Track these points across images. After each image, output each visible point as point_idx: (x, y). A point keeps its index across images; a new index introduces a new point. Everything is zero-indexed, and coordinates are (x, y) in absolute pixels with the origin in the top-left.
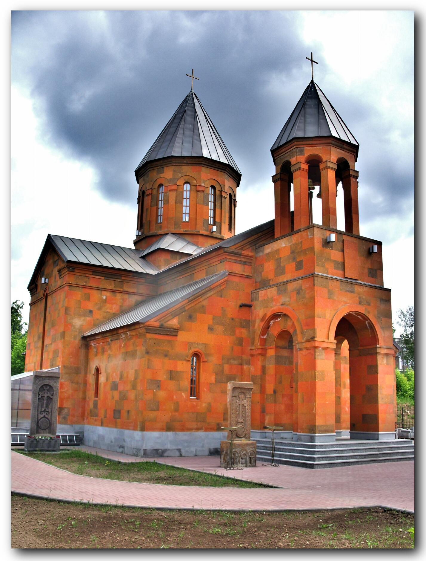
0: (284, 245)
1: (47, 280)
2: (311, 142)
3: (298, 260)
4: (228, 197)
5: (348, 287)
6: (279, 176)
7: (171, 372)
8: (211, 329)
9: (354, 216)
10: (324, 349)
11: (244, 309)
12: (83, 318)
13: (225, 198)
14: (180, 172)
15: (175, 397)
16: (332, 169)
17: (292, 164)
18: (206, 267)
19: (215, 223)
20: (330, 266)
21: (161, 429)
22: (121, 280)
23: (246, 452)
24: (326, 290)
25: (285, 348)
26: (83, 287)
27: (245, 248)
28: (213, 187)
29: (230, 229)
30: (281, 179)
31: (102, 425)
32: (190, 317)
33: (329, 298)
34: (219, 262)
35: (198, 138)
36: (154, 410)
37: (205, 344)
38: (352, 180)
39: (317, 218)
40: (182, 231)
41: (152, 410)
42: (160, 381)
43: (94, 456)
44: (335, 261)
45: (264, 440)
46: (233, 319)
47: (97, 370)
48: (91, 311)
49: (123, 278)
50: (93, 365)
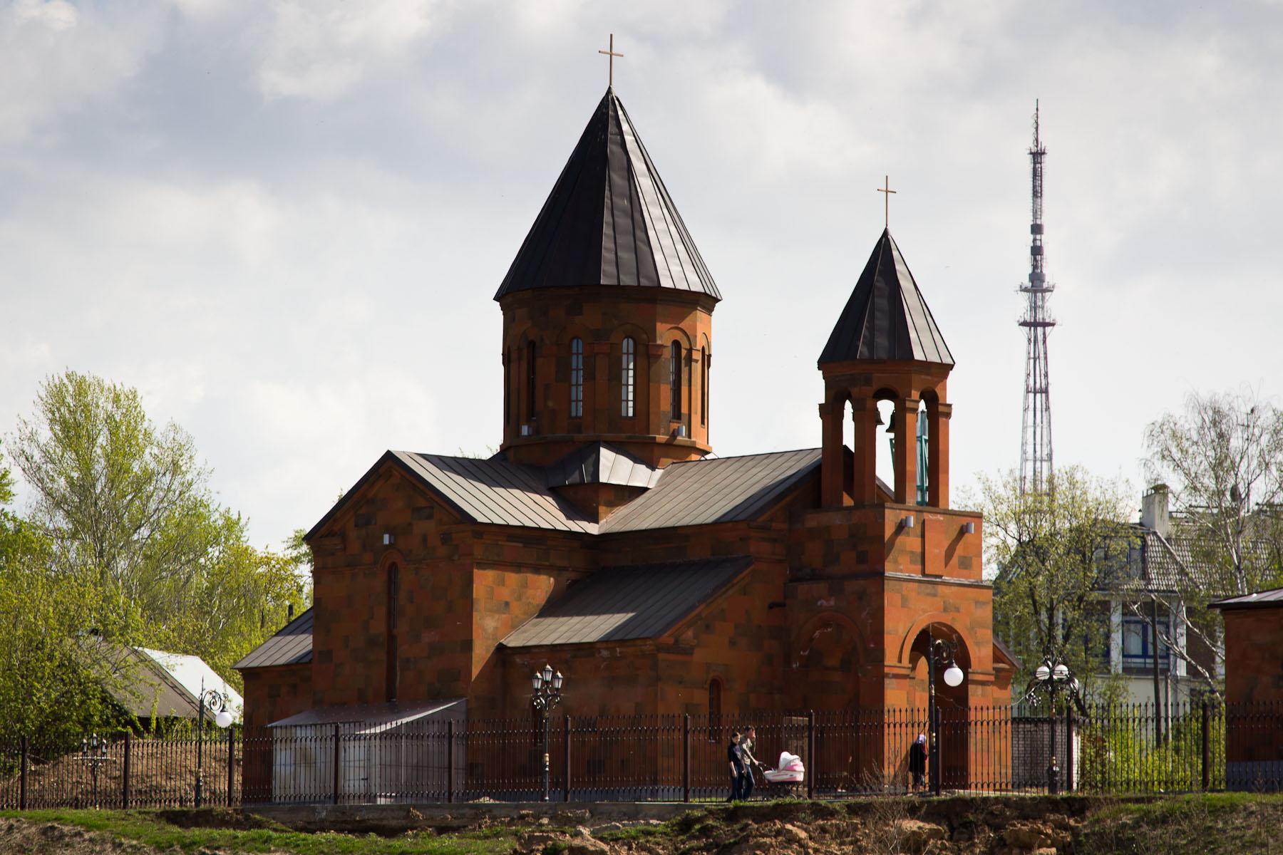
0: (838, 522)
5: (930, 588)
8: (732, 643)
9: (941, 476)
10: (896, 676)
12: (497, 616)
13: (697, 361)
20: (904, 561)
24: (899, 596)
29: (703, 422)
32: (708, 627)
35: (643, 236)
38: (942, 420)
39: (885, 471)
40: (623, 436)
43: (966, 716)
44: (912, 552)
48: (507, 604)
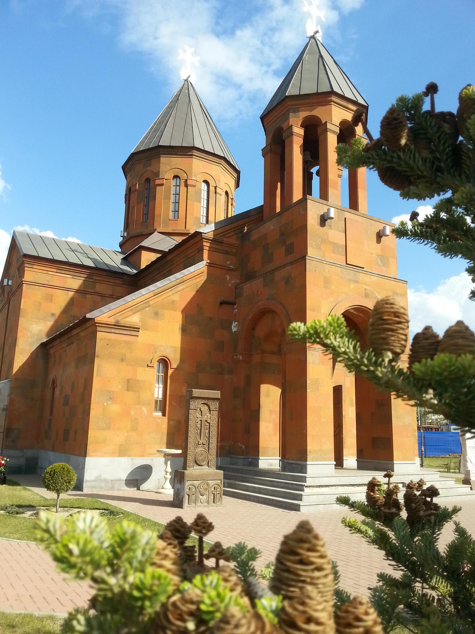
2: (306, 101)
3: (288, 243)
6: (269, 148)
7: (128, 381)
11: (225, 307)
13: (221, 195)
15: (133, 412)
16: (333, 132)
17: (284, 129)
18: (184, 260)
21: (112, 454)
22: (92, 280)
23: (208, 484)
25: (274, 353)
26: (44, 285)
27: (228, 236)
28: (206, 182)
30: (271, 151)
31: (53, 450)
36: (104, 429)
37: (175, 347)
41: (100, 429)
42: (113, 392)
45: (232, 466)
47: (54, 382)
49: (94, 278)
50: (51, 377)
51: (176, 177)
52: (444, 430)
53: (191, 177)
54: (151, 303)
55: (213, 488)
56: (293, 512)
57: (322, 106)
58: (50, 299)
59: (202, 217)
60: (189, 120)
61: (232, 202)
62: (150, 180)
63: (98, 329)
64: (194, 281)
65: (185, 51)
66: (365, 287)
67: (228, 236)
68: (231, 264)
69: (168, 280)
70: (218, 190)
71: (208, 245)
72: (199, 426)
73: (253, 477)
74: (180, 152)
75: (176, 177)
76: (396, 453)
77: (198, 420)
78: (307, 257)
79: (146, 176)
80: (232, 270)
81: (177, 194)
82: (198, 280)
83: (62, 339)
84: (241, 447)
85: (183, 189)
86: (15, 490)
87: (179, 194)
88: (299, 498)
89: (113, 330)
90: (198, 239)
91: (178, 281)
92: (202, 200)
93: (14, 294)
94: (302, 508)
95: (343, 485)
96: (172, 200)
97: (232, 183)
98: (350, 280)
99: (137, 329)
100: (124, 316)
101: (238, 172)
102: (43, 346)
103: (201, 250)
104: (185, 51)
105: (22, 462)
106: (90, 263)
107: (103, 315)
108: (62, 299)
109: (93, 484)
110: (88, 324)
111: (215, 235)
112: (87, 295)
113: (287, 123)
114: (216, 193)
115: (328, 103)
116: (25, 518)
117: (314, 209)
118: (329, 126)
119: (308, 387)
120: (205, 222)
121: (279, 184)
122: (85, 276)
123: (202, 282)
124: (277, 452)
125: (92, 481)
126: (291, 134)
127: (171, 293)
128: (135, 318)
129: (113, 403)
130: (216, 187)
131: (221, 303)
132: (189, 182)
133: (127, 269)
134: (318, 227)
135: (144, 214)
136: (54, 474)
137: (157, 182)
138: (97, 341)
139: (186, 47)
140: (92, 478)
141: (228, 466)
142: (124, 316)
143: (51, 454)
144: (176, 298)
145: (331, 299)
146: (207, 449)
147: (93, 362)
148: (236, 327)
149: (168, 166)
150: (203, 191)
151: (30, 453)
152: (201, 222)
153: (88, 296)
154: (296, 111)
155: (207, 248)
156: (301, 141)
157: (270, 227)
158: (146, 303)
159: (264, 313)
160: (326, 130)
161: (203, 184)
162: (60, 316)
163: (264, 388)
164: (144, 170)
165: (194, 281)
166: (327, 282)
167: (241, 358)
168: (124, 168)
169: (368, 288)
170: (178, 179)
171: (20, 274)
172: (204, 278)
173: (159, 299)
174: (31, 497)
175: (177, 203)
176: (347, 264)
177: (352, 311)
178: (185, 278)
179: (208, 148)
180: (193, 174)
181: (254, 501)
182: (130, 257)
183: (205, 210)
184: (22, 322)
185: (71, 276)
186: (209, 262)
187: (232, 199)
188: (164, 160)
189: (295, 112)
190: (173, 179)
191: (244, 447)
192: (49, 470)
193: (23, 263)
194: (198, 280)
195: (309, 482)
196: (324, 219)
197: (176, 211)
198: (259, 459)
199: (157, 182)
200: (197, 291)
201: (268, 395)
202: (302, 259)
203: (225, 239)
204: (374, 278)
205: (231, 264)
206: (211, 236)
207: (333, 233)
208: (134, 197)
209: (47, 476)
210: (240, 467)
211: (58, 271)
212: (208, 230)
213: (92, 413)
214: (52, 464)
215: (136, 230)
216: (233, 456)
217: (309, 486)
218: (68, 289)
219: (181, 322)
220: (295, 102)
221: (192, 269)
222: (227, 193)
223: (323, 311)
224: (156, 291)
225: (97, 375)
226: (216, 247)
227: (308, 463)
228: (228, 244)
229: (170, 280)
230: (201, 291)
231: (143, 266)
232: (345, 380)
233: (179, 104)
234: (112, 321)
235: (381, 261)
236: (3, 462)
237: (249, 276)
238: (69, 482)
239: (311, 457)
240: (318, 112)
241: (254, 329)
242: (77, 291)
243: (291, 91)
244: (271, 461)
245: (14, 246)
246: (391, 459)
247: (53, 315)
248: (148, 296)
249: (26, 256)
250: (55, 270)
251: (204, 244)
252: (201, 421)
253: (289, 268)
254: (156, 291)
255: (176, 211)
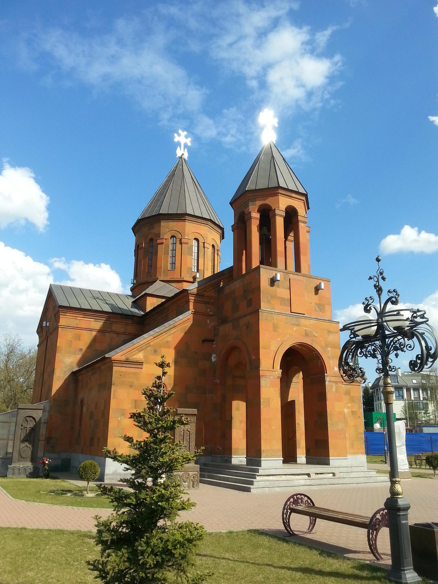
1: (48, 323)
4: (211, 247)
13: (208, 248)
14: (167, 228)
16: (281, 216)
19: (198, 270)
23: (189, 475)
26: (74, 328)
27: (208, 290)
28: (196, 239)
31: (82, 453)
33: (275, 331)
34: (185, 303)
41: (116, 437)
46: (196, 353)
47: (82, 401)
49: (111, 320)
50: (80, 397)
51: (173, 237)
52: (418, 431)
53: (185, 236)
54: (151, 344)
55: (192, 477)
56: (245, 493)
57: (272, 196)
58: (78, 337)
59: (193, 267)
60: (182, 191)
61: (218, 252)
62: (153, 240)
63: (114, 364)
64: (183, 326)
65: (179, 135)
66: (305, 329)
67: (208, 290)
68: (210, 311)
69: (163, 326)
70: (206, 245)
71: (193, 298)
72: (182, 434)
73: (223, 470)
74: (176, 218)
75: (173, 237)
76: (331, 451)
77: (182, 430)
78: (260, 311)
79: (150, 237)
80: (211, 316)
81: (174, 250)
82: (185, 325)
83: (88, 370)
84: (219, 449)
85: (178, 246)
86: (57, 482)
87: (175, 250)
88: (252, 483)
89: (124, 365)
90: (185, 294)
91: (171, 326)
92: (193, 253)
93: (51, 334)
94: (252, 490)
95: (286, 475)
96: (170, 255)
97: (217, 237)
98: (293, 324)
99: (141, 363)
100: (132, 354)
101: (222, 229)
102: (74, 374)
103: (188, 302)
104: (179, 135)
105: (59, 462)
106: (107, 309)
107: (117, 355)
108: (87, 338)
109: (111, 477)
110: (107, 361)
111: (198, 291)
112: (106, 334)
113: (247, 209)
114: (204, 247)
115: (276, 195)
116: (67, 496)
117: (266, 273)
118: (277, 212)
119: (261, 404)
120: (196, 271)
121: (244, 251)
122: (105, 319)
123: (189, 326)
124: (245, 451)
125: (110, 475)
126: (250, 218)
127: (166, 336)
128: (140, 355)
129: (125, 418)
130: (204, 243)
131: (203, 341)
132: (183, 241)
133: (135, 311)
134: (269, 287)
135: (149, 266)
136: (85, 468)
137: (159, 241)
138: (113, 373)
139: (180, 131)
140: (111, 472)
141: (210, 463)
142: (132, 354)
143: (80, 456)
144: (170, 339)
145: (279, 339)
146: (188, 450)
147: (110, 388)
148: (215, 358)
149: (167, 228)
150: (194, 247)
151: (64, 456)
152: (193, 271)
153: (107, 334)
154: (254, 200)
155: (193, 301)
156: (258, 222)
157: (237, 285)
158: (148, 344)
159: (233, 349)
160: (275, 215)
161: (194, 241)
162: (86, 351)
163: (235, 403)
164: (149, 231)
165: (183, 326)
166: (275, 327)
167: (218, 381)
168: (133, 229)
169: (307, 329)
170: (175, 238)
171: (56, 319)
172: (190, 323)
173: (157, 340)
174: (69, 486)
175: (174, 256)
176: (291, 312)
177: (297, 346)
178: (176, 324)
179: (198, 214)
180: (186, 234)
181: (216, 486)
182: (139, 302)
183: (196, 261)
184: (58, 356)
185: (94, 320)
186: (194, 311)
187: (218, 250)
188: (163, 224)
189: (252, 201)
190: (171, 238)
191: (221, 448)
192: (82, 465)
193: (58, 312)
194: (185, 325)
195: (261, 472)
196: (273, 281)
197: (173, 263)
198: (232, 457)
199: (159, 241)
200: (185, 333)
201: (238, 409)
202: (256, 311)
203: (206, 293)
204: (313, 322)
205: (210, 311)
206: (195, 291)
207: (281, 291)
208: (141, 252)
209: (81, 469)
210: (217, 464)
211: (84, 316)
212: (193, 288)
213: (110, 425)
214: (84, 462)
215: (142, 279)
216: (213, 455)
217: (260, 475)
218: (91, 330)
219: (174, 357)
220: (253, 194)
221: (181, 317)
222: (213, 246)
223: (272, 349)
224: (155, 335)
225: (113, 398)
226: (199, 299)
227: (262, 459)
228: (208, 297)
229: (165, 326)
230: (188, 333)
231: (148, 310)
232: (298, 396)
233: (175, 179)
234: (123, 358)
235: (318, 308)
236: (47, 462)
237: (224, 321)
238: (95, 474)
239: (265, 455)
240: (269, 201)
241: (227, 360)
242: (100, 331)
243: (250, 186)
244: (241, 458)
245: (51, 296)
246: (328, 456)
247: (81, 350)
248: (149, 339)
249: (61, 307)
250: (82, 316)
251: (190, 298)
252: (184, 430)
253: (248, 317)
254: (155, 335)
255: (173, 263)
